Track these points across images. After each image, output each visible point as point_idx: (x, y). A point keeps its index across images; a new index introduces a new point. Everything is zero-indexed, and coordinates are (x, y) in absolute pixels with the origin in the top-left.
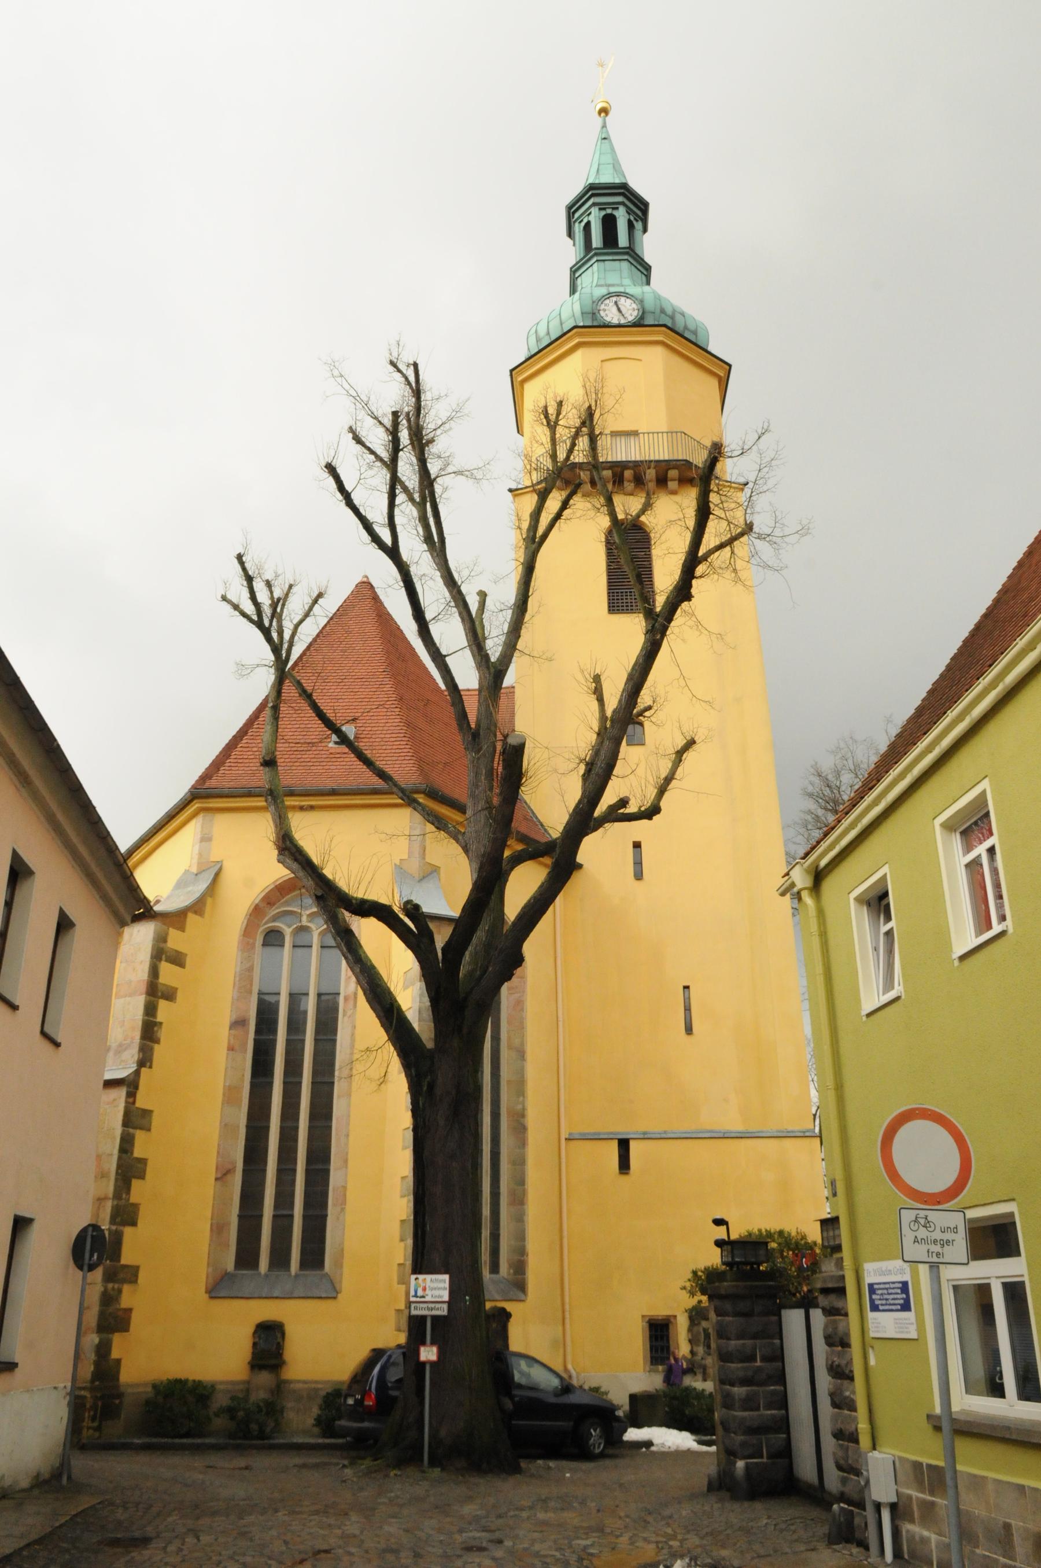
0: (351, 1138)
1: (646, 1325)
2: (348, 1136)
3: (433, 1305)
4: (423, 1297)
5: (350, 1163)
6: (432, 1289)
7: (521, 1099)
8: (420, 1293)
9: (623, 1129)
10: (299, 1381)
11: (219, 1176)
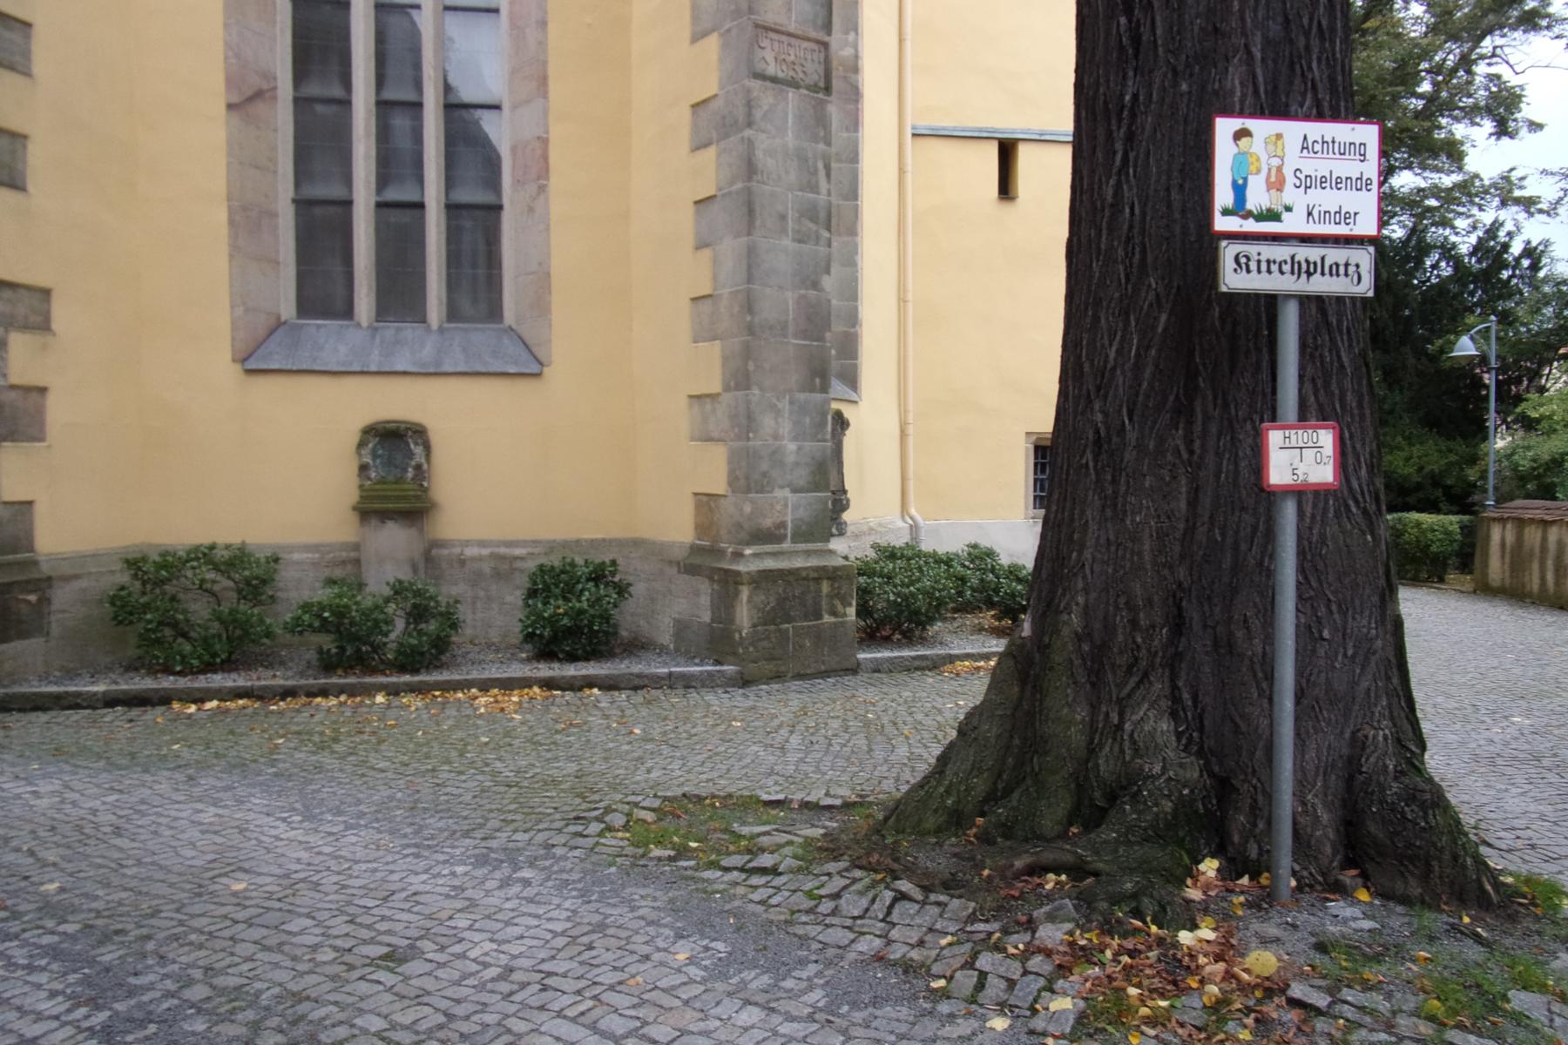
0: (551, 27)
1: (1031, 447)
2: (543, 24)
3: (1313, 253)
4: (1272, 216)
5: (553, 86)
6: (1307, 183)
7: (851, 36)
8: (1257, 198)
9: (1009, 123)
10: (467, 543)
11: (235, 99)
